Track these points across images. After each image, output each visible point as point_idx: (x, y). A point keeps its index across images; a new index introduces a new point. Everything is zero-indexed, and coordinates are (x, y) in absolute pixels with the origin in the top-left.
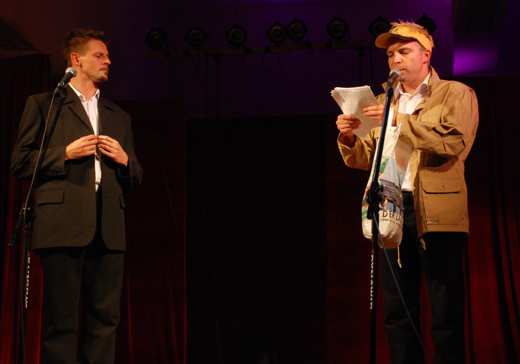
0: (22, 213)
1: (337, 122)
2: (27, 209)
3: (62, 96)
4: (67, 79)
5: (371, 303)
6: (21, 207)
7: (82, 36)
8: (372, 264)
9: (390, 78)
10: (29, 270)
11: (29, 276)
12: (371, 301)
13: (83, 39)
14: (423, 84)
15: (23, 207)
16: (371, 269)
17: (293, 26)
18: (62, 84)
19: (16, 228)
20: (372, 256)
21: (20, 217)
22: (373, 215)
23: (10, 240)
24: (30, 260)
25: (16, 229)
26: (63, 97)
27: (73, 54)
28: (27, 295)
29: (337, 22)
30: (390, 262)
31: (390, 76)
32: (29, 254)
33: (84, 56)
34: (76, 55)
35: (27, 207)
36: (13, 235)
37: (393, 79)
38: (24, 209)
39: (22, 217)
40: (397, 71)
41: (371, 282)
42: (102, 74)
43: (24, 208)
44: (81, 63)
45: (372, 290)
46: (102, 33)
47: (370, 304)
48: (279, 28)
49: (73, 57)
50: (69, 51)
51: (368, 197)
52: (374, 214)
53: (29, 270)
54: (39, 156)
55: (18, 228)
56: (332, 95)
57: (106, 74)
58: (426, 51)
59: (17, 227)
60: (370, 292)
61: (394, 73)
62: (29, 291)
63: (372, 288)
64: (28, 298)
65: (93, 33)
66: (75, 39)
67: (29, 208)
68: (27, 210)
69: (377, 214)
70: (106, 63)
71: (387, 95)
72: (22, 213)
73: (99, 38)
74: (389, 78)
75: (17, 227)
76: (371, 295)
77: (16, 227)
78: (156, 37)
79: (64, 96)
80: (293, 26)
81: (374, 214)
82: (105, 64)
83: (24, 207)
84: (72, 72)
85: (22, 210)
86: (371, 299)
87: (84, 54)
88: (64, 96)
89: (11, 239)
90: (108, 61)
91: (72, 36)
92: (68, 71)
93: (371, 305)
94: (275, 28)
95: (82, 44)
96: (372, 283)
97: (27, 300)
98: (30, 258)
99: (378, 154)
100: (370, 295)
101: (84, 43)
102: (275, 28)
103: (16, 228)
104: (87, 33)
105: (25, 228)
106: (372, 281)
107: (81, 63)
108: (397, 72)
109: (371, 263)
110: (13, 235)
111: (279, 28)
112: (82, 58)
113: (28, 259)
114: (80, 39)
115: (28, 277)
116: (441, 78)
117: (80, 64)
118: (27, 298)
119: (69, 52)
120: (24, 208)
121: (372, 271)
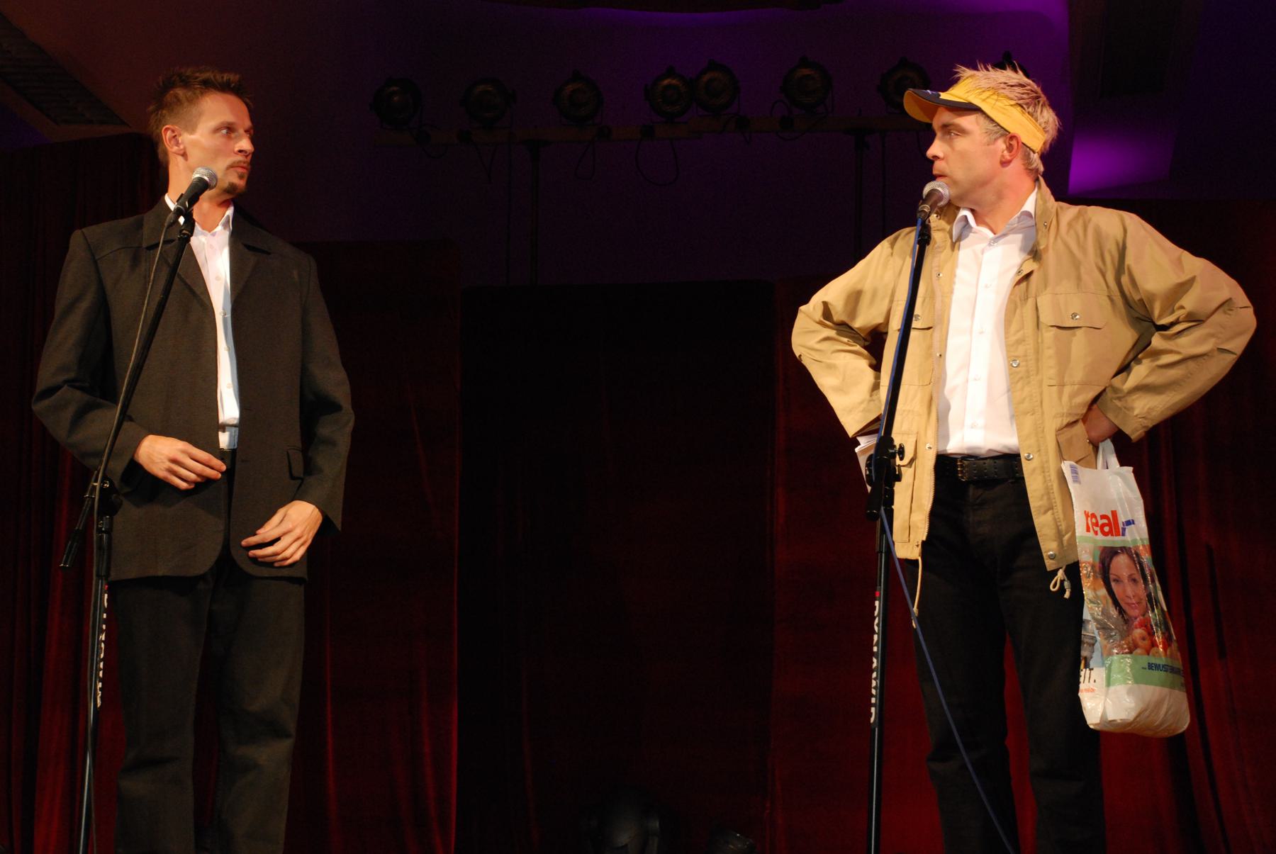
0: (91, 494)
1: (803, 308)
2: (103, 486)
3: (184, 232)
4: (196, 193)
5: (873, 710)
6: (88, 482)
7: (186, 83)
8: (876, 621)
9: (925, 201)
10: (105, 621)
11: (106, 636)
12: (872, 705)
13: (190, 93)
14: (1023, 212)
15: (93, 479)
16: (874, 632)
17: (706, 77)
18: (184, 206)
19: (77, 528)
20: (877, 603)
21: (86, 503)
22: (879, 510)
23: (64, 554)
24: (107, 600)
25: (78, 529)
26: (184, 234)
27: (167, 129)
28: (99, 677)
29: (806, 71)
30: (939, 681)
31: (924, 197)
32: (107, 586)
33: (191, 134)
34: (173, 131)
35: (103, 482)
36: (70, 542)
37: (930, 203)
38: (95, 487)
39: (90, 502)
40: (939, 186)
41: (873, 663)
42: (234, 179)
43: (95, 484)
44: (185, 148)
45: (875, 679)
46: (233, 77)
47: (870, 709)
48: (674, 82)
49: (166, 135)
50: (160, 121)
51: (870, 471)
52: (882, 508)
53: (105, 621)
54: (130, 366)
55: (81, 528)
56: (857, 450)
57: (241, 177)
58: (1009, 136)
59: (79, 526)
60: (871, 683)
61: (933, 192)
62: (104, 669)
63: (874, 675)
64: (102, 685)
65: (212, 77)
66: (172, 92)
67: (106, 483)
68: (102, 489)
69: (888, 508)
70: (242, 149)
71: (916, 242)
72: (91, 494)
73: (224, 88)
74: (921, 201)
75: (79, 526)
76: (874, 692)
77: (78, 525)
78: (395, 98)
79: (187, 232)
80: (706, 77)
81: (882, 508)
82: (240, 151)
83: (96, 481)
84: (206, 178)
85: (90, 487)
86: (873, 700)
87: (192, 129)
88: (187, 232)
89: (66, 553)
90: (245, 144)
91: (169, 85)
92: (198, 176)
93: (872, 713)
94: (666, 82)
95: (186, 104)
96: (875, 665)
97: (100, 689)
98: (108, 596)
99: (894, 374)
100: (871, 690)
101: (191, 101)
102: (666, 82)
103: (77, 528)
104: (201, 79)
105: (97, 527)
106: (875, 660)
107: (185, 148)
108: (940, 189)
109: (875, 618)
110: (70, 542)
111: (674, 82)
112: (186, 138)
113: (104, 598)
114: (180, 92)
115: (103, 639)
116: (1057, 199)
117: (182, 152)
118: (100, 685)
119: (160, 123)
120: (95, 484)
121: (876, 637)
